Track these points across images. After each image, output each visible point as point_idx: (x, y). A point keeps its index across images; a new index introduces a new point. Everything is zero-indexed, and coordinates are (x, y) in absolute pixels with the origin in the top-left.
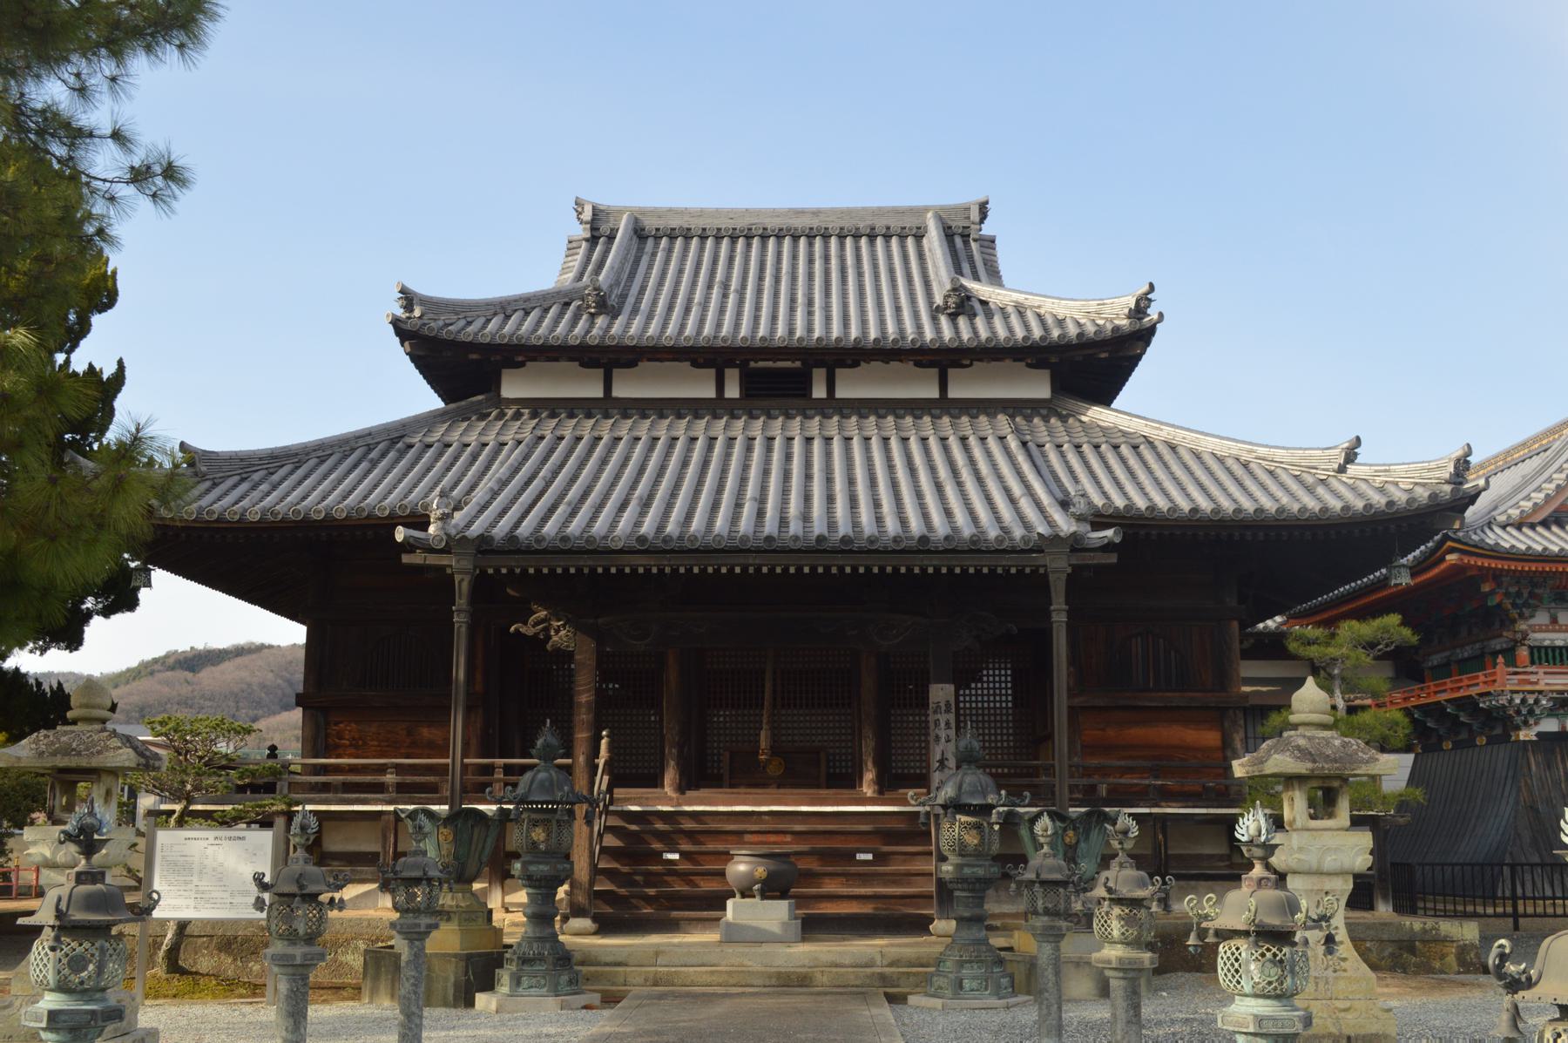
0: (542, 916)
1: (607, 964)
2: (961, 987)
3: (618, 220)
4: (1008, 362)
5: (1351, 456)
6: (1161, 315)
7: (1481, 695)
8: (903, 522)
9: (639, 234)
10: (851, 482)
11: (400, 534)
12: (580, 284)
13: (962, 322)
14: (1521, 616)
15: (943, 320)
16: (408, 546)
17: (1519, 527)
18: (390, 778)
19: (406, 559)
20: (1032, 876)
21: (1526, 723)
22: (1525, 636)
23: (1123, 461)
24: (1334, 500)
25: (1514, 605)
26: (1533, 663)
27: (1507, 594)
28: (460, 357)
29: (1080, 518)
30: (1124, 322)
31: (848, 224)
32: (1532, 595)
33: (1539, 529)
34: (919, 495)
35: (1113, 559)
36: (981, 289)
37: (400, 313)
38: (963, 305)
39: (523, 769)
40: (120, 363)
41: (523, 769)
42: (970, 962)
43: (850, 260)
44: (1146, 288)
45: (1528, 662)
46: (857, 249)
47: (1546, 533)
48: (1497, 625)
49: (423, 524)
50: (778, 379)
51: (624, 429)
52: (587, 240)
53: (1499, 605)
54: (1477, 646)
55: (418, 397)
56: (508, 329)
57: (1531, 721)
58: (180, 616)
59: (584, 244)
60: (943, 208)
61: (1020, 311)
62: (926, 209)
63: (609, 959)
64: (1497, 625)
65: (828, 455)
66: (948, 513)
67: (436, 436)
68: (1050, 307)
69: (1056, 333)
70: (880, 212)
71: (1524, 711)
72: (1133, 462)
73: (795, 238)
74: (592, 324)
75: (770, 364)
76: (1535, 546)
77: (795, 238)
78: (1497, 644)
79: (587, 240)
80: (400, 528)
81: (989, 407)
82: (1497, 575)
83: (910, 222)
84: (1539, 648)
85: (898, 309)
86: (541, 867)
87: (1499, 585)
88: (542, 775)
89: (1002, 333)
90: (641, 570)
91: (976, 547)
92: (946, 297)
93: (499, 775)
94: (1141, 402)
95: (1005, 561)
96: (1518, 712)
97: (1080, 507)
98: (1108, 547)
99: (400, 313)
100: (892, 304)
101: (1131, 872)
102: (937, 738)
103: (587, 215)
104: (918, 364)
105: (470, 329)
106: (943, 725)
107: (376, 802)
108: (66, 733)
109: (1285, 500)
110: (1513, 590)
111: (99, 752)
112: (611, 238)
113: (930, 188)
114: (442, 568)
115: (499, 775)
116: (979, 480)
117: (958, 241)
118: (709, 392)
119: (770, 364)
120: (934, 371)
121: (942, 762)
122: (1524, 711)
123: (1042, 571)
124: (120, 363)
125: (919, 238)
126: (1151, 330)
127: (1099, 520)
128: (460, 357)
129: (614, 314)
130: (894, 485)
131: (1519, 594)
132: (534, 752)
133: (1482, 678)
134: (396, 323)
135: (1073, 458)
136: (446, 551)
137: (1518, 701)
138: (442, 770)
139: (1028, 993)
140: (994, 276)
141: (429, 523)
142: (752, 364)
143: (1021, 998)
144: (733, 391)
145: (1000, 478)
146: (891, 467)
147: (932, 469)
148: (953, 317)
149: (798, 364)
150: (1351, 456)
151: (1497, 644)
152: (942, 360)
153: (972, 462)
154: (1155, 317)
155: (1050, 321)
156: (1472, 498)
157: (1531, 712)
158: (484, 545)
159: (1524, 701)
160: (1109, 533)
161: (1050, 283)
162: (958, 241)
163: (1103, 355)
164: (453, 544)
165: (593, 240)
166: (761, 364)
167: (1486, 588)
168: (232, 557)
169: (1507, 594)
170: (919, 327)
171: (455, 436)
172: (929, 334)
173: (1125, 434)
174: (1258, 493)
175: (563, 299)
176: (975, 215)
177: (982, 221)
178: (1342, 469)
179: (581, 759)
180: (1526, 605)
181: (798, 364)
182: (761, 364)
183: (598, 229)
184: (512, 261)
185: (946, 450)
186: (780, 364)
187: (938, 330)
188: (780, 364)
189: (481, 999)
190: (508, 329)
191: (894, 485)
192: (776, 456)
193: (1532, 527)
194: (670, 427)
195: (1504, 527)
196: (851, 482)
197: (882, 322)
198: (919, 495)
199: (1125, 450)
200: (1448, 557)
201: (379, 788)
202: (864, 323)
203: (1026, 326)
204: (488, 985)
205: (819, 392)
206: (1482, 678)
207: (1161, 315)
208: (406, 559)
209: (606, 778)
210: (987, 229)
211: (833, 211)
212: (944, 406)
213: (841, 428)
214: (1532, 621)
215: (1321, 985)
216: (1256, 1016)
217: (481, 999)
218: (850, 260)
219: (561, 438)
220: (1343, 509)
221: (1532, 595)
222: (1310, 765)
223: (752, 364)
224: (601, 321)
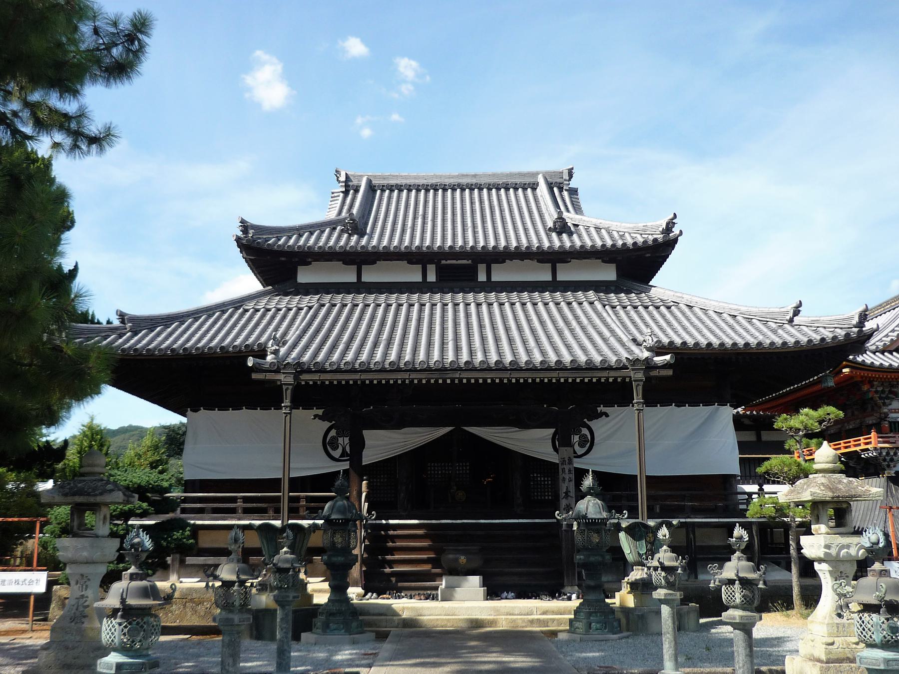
0: (339, 589)
1: (374, 615)
2: (590, 628)
3: (360, 180)
4: (517, 262)
5: (796, 312)
6: (681, 232)
7: (863, 450)
8: (500, 353)
9: (372, 189)
10: (507, 330)
11: (250, 362)
12: (341, 217)
13: (565, 236)
14: (884, 404)
15: (554, 235)
16: (255, 369)
17: (883, 352)
18: (240, 504)
19: (254, 376)
20: (657, 564)
21: (889, 466)
22: (886, 415)
23: (663, 316)
24: (790, 336)
25: (880, 398)
26: (891, 431)
27: (877, 392)
28: (274, 259)
29: (649, 349)
30: (660, 237)
31: (492, 181)
32: (890, 392)
33: (894, 353)
34: (549, 337)
35: (670, 372)
36: (571, 217)
37: (240, 234)
38: (562, 227)
39: (326, 500)
40: (76, 267)
41: (326, 500)
42: (595, 612)
43: (495, 203)
44: (672, 216)
45: (888, 430)
46: (498, 196)
47: (890, 356)
48: (870, 409)
49: (264, 356)
50: (458, 271)
51: (306, 301)
52: (342, 192)
53: (872, 398)
54: (858, 421)
55: (247, 283)
56: (301, 242)
57: (892, 464)
58: (115, 409)
59: (342, 195)
60: (547, 173)
61: (598, 229)
62: (538, 174)
63: (377, 611)
64: (870, 409)
65: (491, 314)
66: (568, 347)
67: (261, 305)
68: (614, 225)
69: (620, 242)
70: (511, 175)
71: (888, 458)
72: (668, 316)
73: (463, 190)
74: (349, 239)
75: (454, 262)
76: (893, 363)
77: (436, 190)
78: (870, 421)
79: (342, 192)
80: (251, 358)
81: (584, 286)
82: (870, 382)
83: (528, 180)
84: (895, 423)
85: (526, 230)
86: (339, 558)
87: (872, 386)
88: (340, 503)
89: (578, 244)
90: (522, 381)
91: (590, 367)
92: (555, 223)
93: (303, 503)
94: (666, 281)
95: (489, 375)
96: (885, 460)
97: (650, 342)
98: (666, 366)
99: (240, 234)
100: (525, 225)
101: (745, 563)
102: (564, 479)
103: (343, 178)
104: (539, 261)
105: (280, 243)
106: (567, 471)
107: (232, 518)
108: (80, 482)
109: (761, 338)
110: (880, 389)
111: (101, 494)
112: (357, 191)
113: (541, 163)
114: (274, 381)
115: (303, 503)
116: (583, 328)
117: (556, 190)
118: (418, 278)
119: (454, 262)
120: (549, 266)
121: (567, 493)
122: (888, 458)
123: (627, 380)
124: (76, 267)
125: (534, 189)
126: (675, 241)
127: (659, 349)
128: (274, 259)
129: (362, 234)
130: (533, 331)
131: (883, 392)
132: (333, 489)
133: (863, 441)
134: (238, 240)
135: (633, 313)
136: (277, 371)
137: (884, 454)
138: (278, 499)
139: (628, 630)
140: (578, 209)
141: (266, 355)
142: (443, 262)
143: (625, 634)
144: (432, 277)
145: (595, 327)
146: (529, 321)
147: (554, 322)
148: (559, 234)
149: (470, 262)
150: (796, 312)
151: (870, 421)
152: (553, 258)
153: (576, 318)
154: (677, 232)
155: (615, 234)
156: (870, 336)
157: (892, 460)
158: (300, 369)
159: (888, 454)
160: (668, 357)
161: (612, 217)
162: (556, 190)
163: (648, 255)
164: (277, 369)
165: (346, 193)
166: (449, 262)
167: (865, 388)
168: (144, 374)
169: (877, 392)
170: (539, 240)
171: (272, 305)
172: (546, 244)
173: (662, 301)
174: (745, 334)
175: (332, 225)
176: (566, 177)
177: (570, 180)
178: (791, 321)
179: (355, 493)
180: (887, 398)
181: (470, 262)
182: (449, 262)
183: (349, 187)
184: (298, 205)
185: (560, 311)
186: (460, 262)
187: (550, 241)
188: (460, 262)
189: (304, 635)
190: (301, 242)
191: (533, 331)
192: (462, 314)
193: (891, 353)
194: (397, 299)
195: (874, 353)
196: (507, 330)
197: (496, 238)
198: (549, 337)
199: (663, 309)
200: (844, 370)
201: (232, 511)
202: (496, 238)
203: (602, 238)
204: (309, 628)
205: (482, 277)
206: (863, 441)
207: (681, 232)
208: (254, 376)
209: (367, 504)
210: (573, 184)
211: (485, 175)
212: (554, 286)
213: (497, 298)
214: (890, 407)
215: (840, 629)
216: (885, 659)
217: (304, 635)
218: (495, 203)
219: (335, 305)
220: (720, 344)
221: (890, 392)
222: (830, 494)
223: (443, 262)
224: (355, 238)
